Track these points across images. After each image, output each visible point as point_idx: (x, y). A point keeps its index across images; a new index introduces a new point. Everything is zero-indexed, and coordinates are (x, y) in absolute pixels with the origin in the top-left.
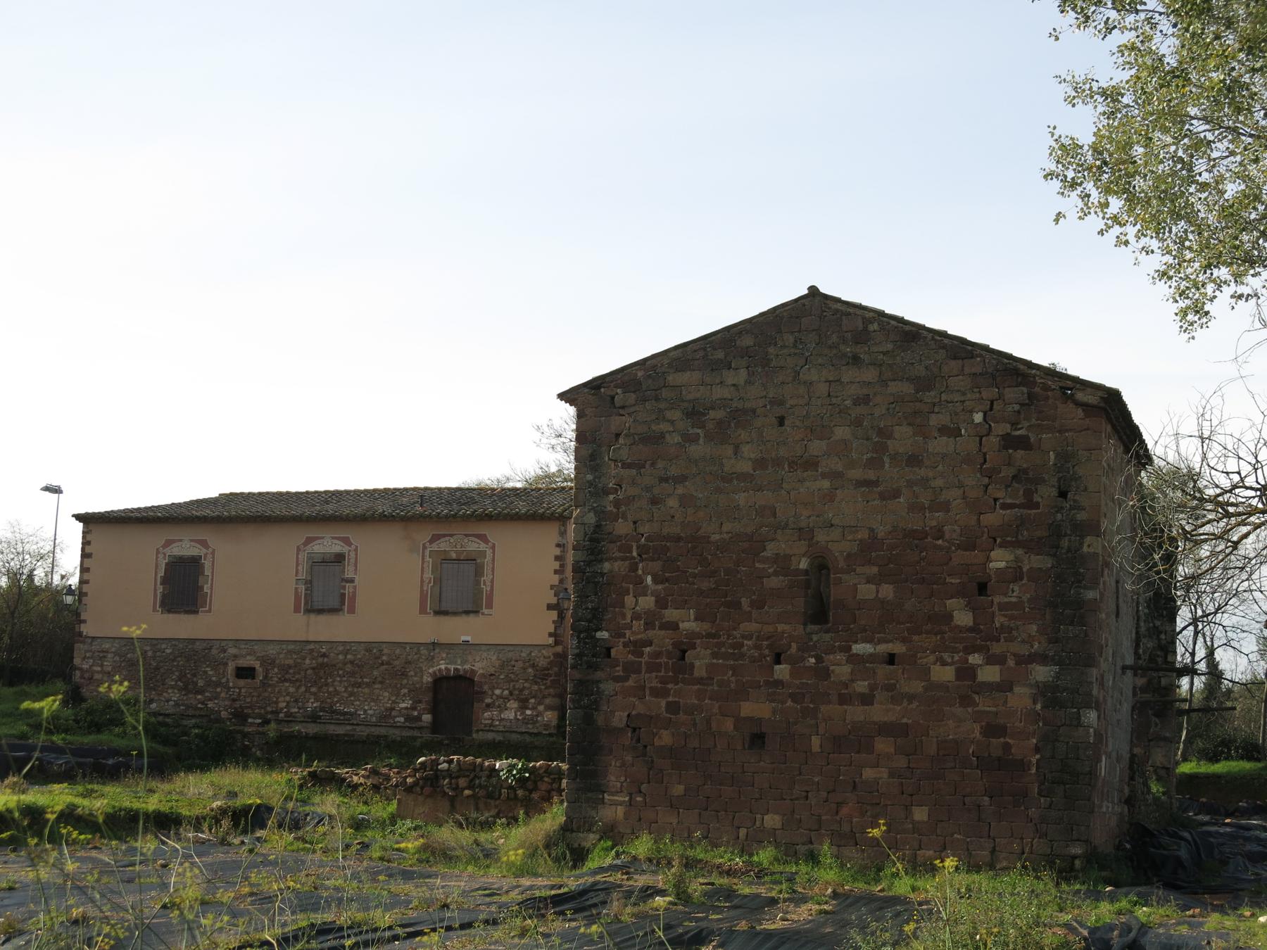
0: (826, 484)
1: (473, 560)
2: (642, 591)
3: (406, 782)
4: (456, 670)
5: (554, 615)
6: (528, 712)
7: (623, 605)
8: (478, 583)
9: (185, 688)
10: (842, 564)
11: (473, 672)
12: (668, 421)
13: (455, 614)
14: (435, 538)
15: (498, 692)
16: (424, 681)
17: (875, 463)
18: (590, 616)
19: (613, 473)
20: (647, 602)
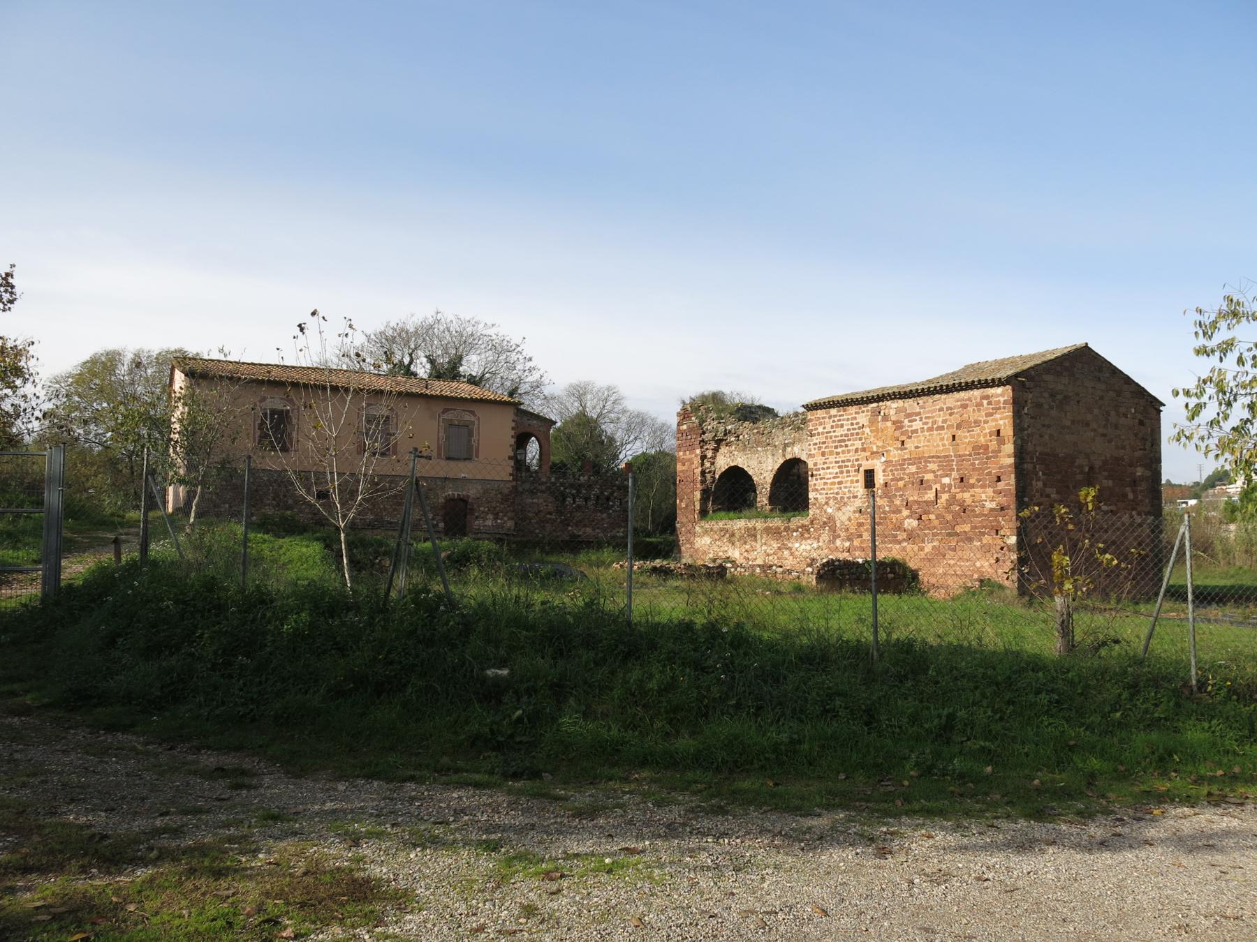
0: (1092, 434)
1: (467, 426)
2: (1038, 480)
4: (458, 495)
5: (512, 463)
6: (499, 521)
7: (1032, 485)
8: (470, 441)
9: (278, 505)
10: (1097, 471)
11: (468, 496)
13: (458, 459)
14: (445, 411)
15: (482, 509)
16: (440, 501)
17: (1105, 426)
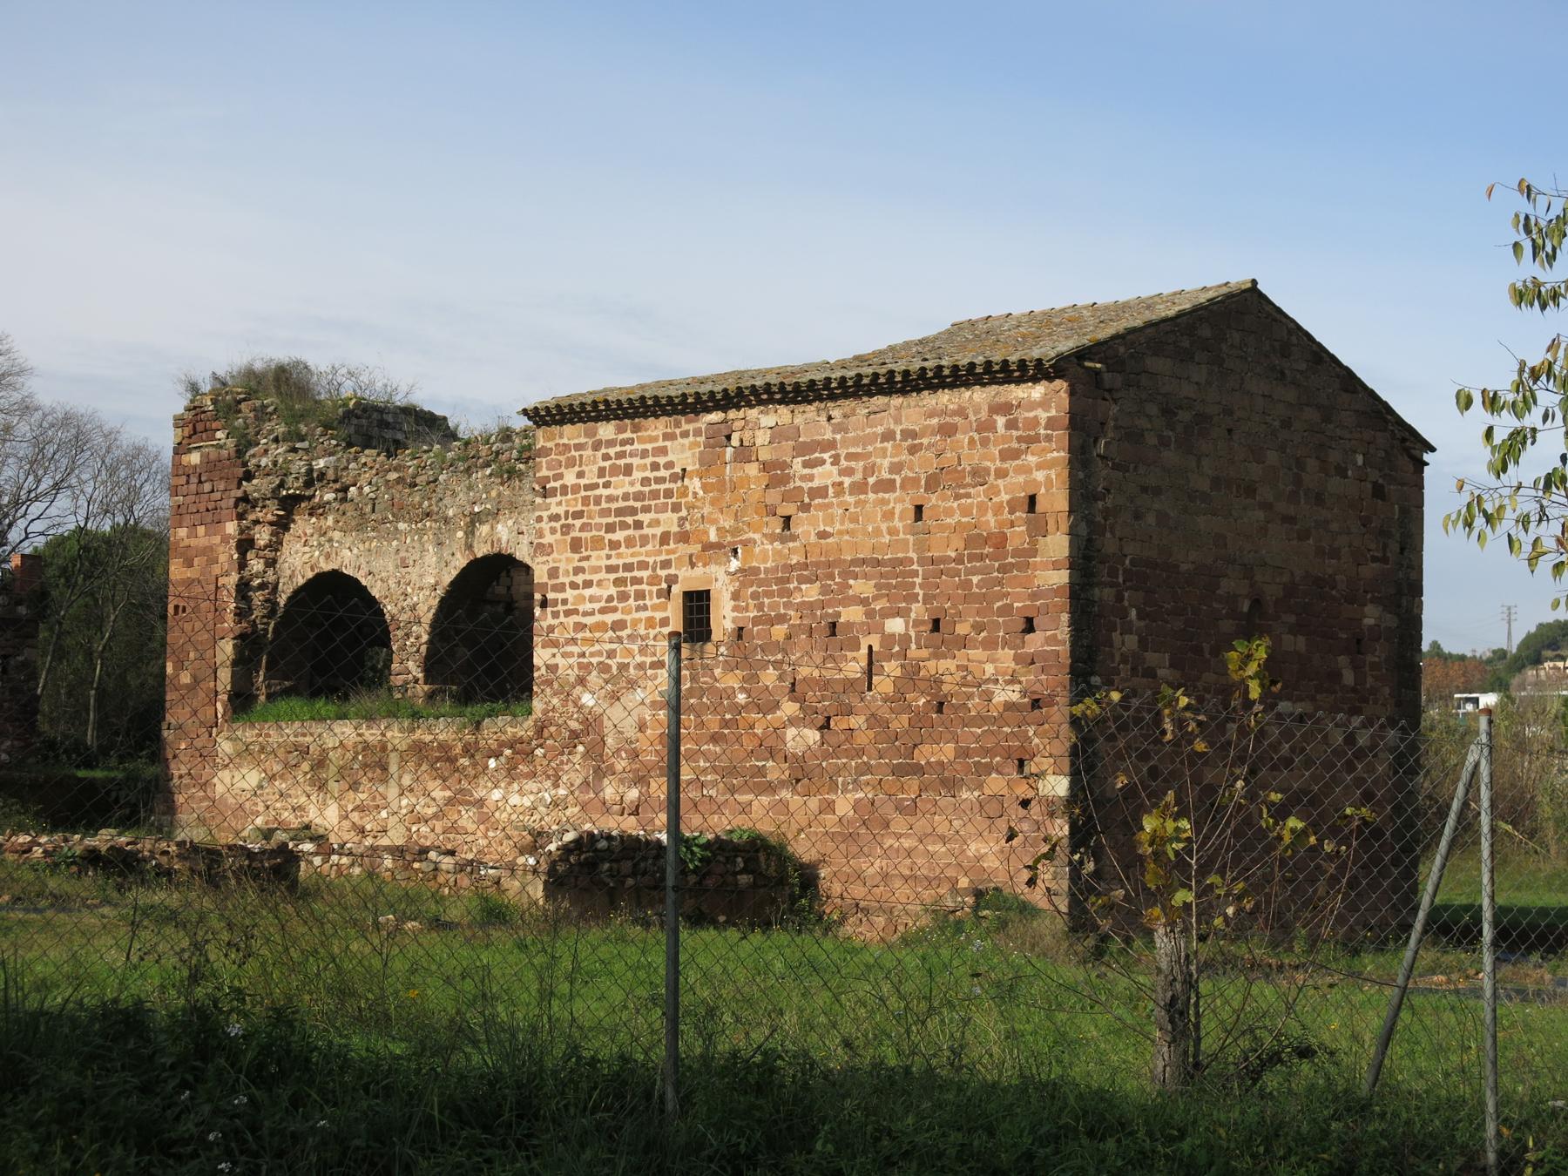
3: (556, 870)
12: (1147, 416)
18: (1086, 657)
19: (1103, 472)
20: (1131, 642)
